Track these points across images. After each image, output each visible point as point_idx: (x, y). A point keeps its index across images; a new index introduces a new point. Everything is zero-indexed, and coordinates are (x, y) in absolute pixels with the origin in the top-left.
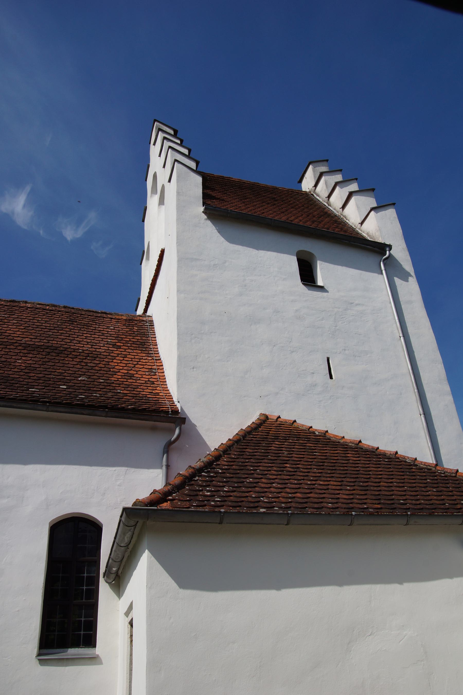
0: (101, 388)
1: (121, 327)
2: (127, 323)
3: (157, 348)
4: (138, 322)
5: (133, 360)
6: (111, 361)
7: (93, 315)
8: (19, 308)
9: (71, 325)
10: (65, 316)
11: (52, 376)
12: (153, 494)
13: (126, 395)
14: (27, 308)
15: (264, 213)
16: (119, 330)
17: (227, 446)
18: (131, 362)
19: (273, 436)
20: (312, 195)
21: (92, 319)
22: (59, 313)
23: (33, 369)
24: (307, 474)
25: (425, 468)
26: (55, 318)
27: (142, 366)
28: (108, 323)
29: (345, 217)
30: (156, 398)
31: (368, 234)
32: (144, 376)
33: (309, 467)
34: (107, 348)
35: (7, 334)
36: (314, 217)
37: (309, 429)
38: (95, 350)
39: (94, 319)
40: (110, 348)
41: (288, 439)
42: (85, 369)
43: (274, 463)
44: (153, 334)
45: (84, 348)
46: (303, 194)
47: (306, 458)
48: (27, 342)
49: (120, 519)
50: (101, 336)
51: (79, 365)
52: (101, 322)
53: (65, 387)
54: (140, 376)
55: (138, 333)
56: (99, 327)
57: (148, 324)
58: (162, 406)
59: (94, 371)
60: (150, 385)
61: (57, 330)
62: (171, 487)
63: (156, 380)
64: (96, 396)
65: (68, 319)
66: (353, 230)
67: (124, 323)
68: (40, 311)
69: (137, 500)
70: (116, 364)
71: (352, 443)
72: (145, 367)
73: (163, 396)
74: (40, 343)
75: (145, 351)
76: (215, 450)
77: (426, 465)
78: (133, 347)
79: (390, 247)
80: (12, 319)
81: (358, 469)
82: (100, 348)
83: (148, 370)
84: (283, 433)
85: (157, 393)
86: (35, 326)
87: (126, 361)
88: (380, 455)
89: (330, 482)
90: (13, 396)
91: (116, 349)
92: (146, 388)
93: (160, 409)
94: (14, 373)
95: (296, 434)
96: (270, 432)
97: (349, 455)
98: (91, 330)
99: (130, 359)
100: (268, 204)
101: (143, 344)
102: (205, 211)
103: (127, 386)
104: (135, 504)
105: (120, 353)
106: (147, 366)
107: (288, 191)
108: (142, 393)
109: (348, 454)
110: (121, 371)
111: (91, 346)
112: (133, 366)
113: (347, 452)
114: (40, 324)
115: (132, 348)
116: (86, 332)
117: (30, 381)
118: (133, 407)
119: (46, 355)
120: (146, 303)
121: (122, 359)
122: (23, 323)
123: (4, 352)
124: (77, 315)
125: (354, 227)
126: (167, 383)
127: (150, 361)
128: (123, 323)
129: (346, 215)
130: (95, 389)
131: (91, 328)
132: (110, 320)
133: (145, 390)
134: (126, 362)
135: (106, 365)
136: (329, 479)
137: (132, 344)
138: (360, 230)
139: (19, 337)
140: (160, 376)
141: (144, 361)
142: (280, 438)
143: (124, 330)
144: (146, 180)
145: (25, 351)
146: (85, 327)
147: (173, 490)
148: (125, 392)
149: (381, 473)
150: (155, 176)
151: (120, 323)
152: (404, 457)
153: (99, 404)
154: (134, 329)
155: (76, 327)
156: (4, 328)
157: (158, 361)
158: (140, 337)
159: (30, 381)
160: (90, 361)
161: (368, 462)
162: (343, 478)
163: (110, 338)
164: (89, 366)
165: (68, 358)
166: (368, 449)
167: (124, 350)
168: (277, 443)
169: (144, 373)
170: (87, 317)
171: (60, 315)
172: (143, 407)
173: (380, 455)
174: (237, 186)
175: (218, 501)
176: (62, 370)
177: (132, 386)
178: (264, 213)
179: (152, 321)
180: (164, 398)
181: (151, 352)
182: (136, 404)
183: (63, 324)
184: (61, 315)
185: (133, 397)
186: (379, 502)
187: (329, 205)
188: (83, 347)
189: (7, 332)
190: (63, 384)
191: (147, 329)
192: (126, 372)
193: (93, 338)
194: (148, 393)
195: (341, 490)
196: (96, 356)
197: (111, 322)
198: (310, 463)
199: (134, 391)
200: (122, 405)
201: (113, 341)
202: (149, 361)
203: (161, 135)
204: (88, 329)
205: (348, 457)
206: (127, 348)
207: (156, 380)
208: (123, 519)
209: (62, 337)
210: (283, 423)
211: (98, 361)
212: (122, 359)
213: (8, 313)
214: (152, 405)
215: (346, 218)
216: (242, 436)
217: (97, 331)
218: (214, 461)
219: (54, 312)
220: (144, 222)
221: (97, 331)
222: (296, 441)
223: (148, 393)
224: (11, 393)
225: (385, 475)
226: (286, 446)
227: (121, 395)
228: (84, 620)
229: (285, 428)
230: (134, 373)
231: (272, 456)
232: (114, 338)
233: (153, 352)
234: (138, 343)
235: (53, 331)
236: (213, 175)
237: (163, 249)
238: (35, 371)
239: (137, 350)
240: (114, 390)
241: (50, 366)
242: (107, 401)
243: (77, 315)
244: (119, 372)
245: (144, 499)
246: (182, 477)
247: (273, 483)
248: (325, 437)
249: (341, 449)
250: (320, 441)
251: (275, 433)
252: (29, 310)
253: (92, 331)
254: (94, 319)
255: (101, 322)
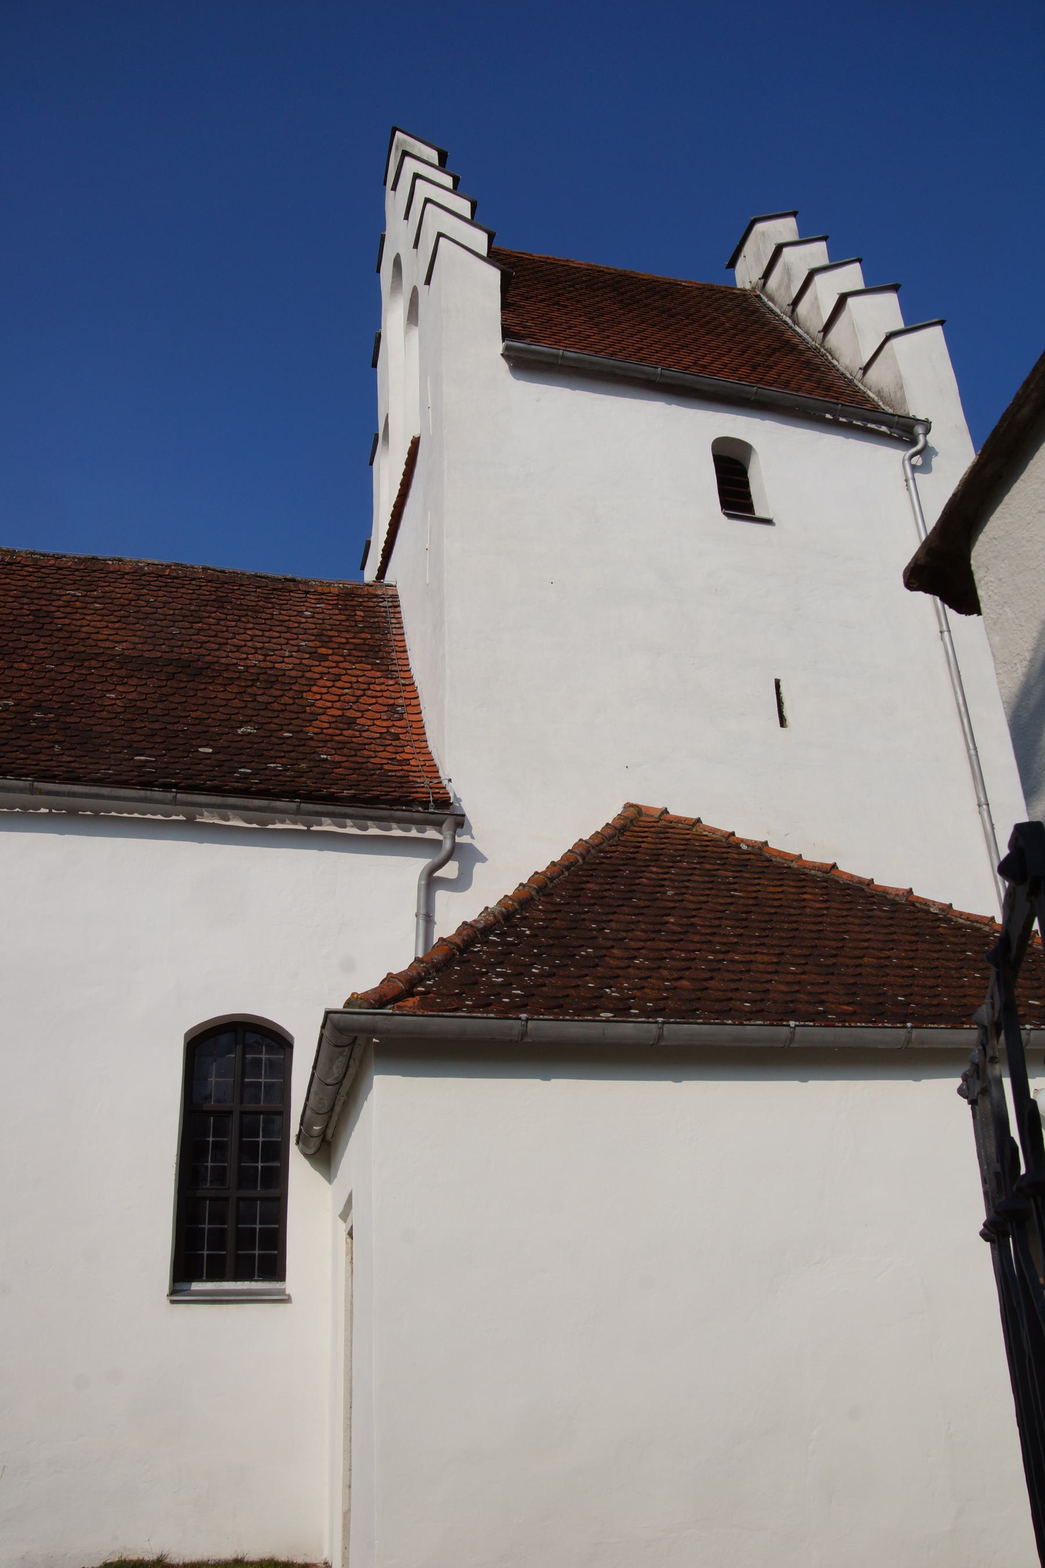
0: (285, 752)
1: (328, 612)
2: (341, 602)
3: (406, 657)
4: (366, 599)
5: (355, 685)
6: (306, 688)
7: (266, 587)
8: (105, 575)
9: (220, 610)
10: (207, 591)
11: (180, 727)
12: (386, 981)
13: (338, 764)
14: (124, 575)
15: (642, 349)
16: (323, 620)
17: (547, 877)
18: (351, 690)
19: (647, 854)
20: (758, 297)
21: (264, 596)
22: (194, 582)
23: (140, 712)
24: (709, 938)
25: (966, 927)
26: (184, 596)
27: (374, 701)
28: (299, 604)
29: (830, 353)
30: (402, 770)
31: (879, 393)
32: (377, 722)
33: (717, 922)
34: (298, 662)
35: (83, 635)
36: (758, 353)
37: (729, 837)
38: (271, 665)
39: (269, 594)
40: (304, 661)
41: (680, 861)
42: (250, 708)
43: (642, 914)
44: (397, 626)
45: (249, 663)
46: (738, 296)
47: (713, 903)
48: (126, 651)
49: (321, 1031)
50: (285, 634)
51: (239, 700)
52: (284, 602)
53: (210, 751)
54: (370, 723)
55: (366, 624)
56: (280, 614)
57: (385, 604)
58: (414, 790)
59: (270, 714)
60: (390, 742)
61: (189, 622)
62: (423, 967)
63: (404, 731)
64: (274, 769)
65: (213, 597)
66: (850, 382)
67: (335, 602)
68: (152, 579)
69: (353, 994)
70: (318, 697)
71: (818, 871)
72: (380, 700)
73: (418, 766)
74: (154, 652)
75: (379, 667)
76: (521, 887)
77: (970, 921)
78: (355, 656)
79: (927, 425)
80: (92, 600)
81: (821, 928)
82: (283, 662)
83: (386, 709)
84: (670, 847)
85: (404, 760)
86: (141, 616)
87: (339, 690)
88: (873, 897)
89: (757, 955)
90: (102, 773)
91: (317, 663)
92: (382, 748)
93: (410, 796)
94: (101, 721)
95: (699, 848)
96: (643, 845)
97: (805, 896)
98: (263, 621)
99: (348, 685)
100: (654, 325)
101: (377, 649)
102: (506, 353)
103: (341, 746)
104: (348, 1004)
105: (326, 670)
106: (386, 700)
107: (702, 289)
108: (372, 760)
109: (805, 893)
110: (329, 712)
111: (263, 657)
112: (353, 699)
113: (804, 890)
114: (153, 610)
115: (353, 659)
116: (251, 625)
117: (135, 738)
118: (353, 792)
119: (167, 680)
120: (382, 555)
121: (330, 684)
122: (116, 608)
123: (77, 676)
124: (231, 587)
125: (848, 375)
126: (428, 735)
127: (391, 688)
128: (331, 602)
129: (833, 349)
130: (272, 753)
131: (264, 616)
132: (304, 595)
133: (380, 753)
134: (340, 692)
135: (297, 698)
136: (753, 950)
137: (352, 650)
138: (862, 383)
139: (107, 640)
140: (412, 721)
141: (378, 688)
142: (662, 857)
143: (334, 617)
144: (378, 271)
145: (123, 672)
146: (249, 613)
147: (427, 972)
148: (337, 758)
149: (868, 936)
150: (397, 263)
151: (326, 601)
152: (926, 902)
153: (281, 787)
154: (355, 615)
155: (229, 615)
156: (74, 622)
157: (408, 689)
158: (368, 633)
159: (135, 738)
160: (260, 692)
161: (845, 913)
162: (784, 946)
163: (305, 636)
164: (259, 702)
165: (214, 684)
166: (849, 884)
167: (334, 665)
168: (655, 869)
169: (378, 716)
170: (253, 592)
171: (195, 587)
172: (375, 793)
173: (873, 897)
174: (585, 281)
175: (518, 996)
176: (202, 712)
177: (353, 744)
178: (642, 349)
179: (396, 596)
180: (420, 771)
181: (394, 668)
182: (359, 785)
183: (202, 608)
184: (198, 588)
185: (354, 769)
186: (851, 1001)
187: (794, 324)
188: (246, 659)
189: (82, 630)
190: (204, 743)
191: (384, 614)
192: (340, 713)
193: (268, 639)
194: (386, 761)
195: (776, 972)
196: (273, 679)
197: (306, 602)
198: (720, 915)
199: (355, 755)
200: (330, 788)
201: (310, 644)
202: (389, 688)
203: (411, 166)
204: (257, 618)
205: (804, 900)
206: (342, 659)
207: (404, 731)
208: (326, 1033)
209: (201, 637)
210: (673, 825)
211: (279, 690)
212: (331, 685)
213: (82, 588)
214: (394, 787)
215: (832, 356)
216: (581, 855)
217: (277, 623)
218: (517, 910)
219: (181, 582)
220: (376, 367)
221: (277, 623)
222: (695, 866)
223: (386, 761)
224: (96, 767)
225: (878, 940)
226: (672, 876)
227: (328, 766)
228: (259, 1228)
229: (677, 836)
230: (355, 716)
231: (639, 899)
232: (313, 638)
233: (398, 668)
234: (366, 648)
235: (181, 624)
236: (531, 255)
237: (417, 436)
238: (145, 716)
239: (362, 664)
240: (313, 755)
241: (178, 703)
242: (297, 779)
243: (231, 587)
244: (324, 714)
245: (367, 992)
246: (446, 945)
247: (635, 958)
248: (761, 855)
249: (792, 883)
250: (747, 865)
251: (653, 846)
252: (126, 579)
253: (265, 624)
254: (269, 594)
255: (284, 602)
